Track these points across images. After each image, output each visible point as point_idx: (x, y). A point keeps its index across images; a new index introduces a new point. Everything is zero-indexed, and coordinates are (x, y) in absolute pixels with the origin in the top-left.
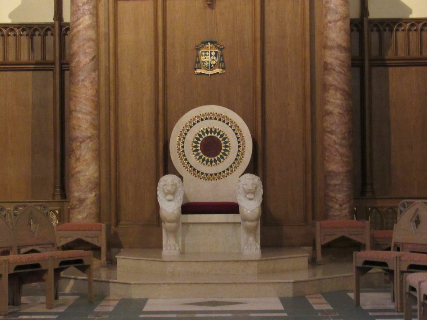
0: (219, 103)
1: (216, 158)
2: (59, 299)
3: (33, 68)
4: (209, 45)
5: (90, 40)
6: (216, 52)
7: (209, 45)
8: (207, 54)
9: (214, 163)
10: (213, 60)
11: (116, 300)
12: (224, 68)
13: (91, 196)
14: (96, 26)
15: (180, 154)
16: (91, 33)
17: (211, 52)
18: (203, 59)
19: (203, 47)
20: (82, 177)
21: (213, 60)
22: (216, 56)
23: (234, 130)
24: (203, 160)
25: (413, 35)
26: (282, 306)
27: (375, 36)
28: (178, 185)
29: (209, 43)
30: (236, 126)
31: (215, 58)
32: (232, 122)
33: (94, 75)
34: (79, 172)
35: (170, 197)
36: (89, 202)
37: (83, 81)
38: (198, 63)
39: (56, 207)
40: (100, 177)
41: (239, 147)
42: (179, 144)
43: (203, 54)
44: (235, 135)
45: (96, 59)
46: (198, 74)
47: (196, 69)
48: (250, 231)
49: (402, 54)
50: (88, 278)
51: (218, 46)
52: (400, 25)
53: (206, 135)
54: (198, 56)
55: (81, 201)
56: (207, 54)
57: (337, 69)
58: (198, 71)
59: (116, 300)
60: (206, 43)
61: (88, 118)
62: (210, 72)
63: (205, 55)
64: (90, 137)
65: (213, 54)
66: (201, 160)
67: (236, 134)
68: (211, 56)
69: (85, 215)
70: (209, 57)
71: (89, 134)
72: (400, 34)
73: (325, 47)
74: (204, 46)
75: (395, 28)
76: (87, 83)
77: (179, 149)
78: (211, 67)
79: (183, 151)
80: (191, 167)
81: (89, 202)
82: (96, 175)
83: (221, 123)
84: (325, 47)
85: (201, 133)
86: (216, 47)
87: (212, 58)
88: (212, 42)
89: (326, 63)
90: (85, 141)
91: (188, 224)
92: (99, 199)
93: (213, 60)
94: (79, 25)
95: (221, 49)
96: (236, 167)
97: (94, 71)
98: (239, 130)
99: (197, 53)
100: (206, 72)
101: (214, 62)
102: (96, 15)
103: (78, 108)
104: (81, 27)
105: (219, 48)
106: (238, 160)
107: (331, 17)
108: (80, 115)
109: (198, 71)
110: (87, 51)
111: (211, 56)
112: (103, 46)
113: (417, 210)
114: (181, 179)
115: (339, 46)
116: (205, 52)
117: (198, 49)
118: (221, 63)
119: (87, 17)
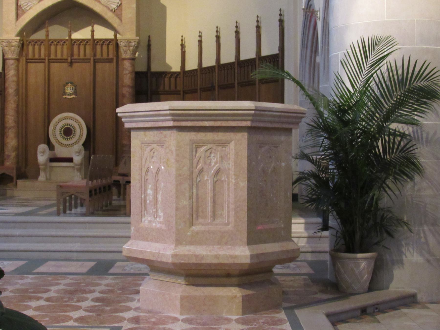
1: (70, 137)
2: (390, 289)
4: (69, 84)
5: (13, 81)
6: (73, 88)
7: (69, 84)
8: (68, 88)
9: (69, 140)
11: (301, 261)
12: (76, 95)
13: (14, 154)
14: (18, 75)
15: (53, 135)
16: (15, 79)
17: (70, 88)
18: (67, 91)
19: (67, 85)
20: (360, 165)
21: (71, 91)
22: (73, 89)
23: (78, 124)
24: (64, 138)
25: (173, 80)
27: (154, 79)
28: (46, 149)
29: (70, 84)
30: (79, 122)
31: (72, 90)
32: (77, 121)
33: (16, 98)
34: (8, 143)
35: (42, 154)
36: (12, 157)
37: (10, 101)
38: (64, 93)
40: (18, 145)
41: (81, 132)
42: (53, 131)
43: (67, 88)
44: (78, 127)
45: (17, 90)
46: (64, 98)
48: (79, 170)
49: (167, 88)
51: (74, 85)
52: (166, 75)
53: (65, 126)
54: (64, 89)
55: (9, 156)
56: (68, 88)
57: (127, 96)
58: (64, 97)
59: (301, 261)
60: (67, 83)
61: (13, 118)
62: (70, 97)
63: (68, 89)
64: (13, 127)
65: (71, 88)
66: (63, 138)
67: (79, 126)
68: (70, 89)
69: (10, 163)
70: (69, 90)
71: (13, 126)
72: (167, 80)
73: (123, 86)
75: (163, 76)
76: (12, 102)
77: (53, 133)
78: (70, 95)
79: (55, 134)
80: (58, 141)
81: (12, 157)
82: (16, 144)
83: (72, 121)
84: (123, 86)
85: (63, 126)
86: (73, 85)
87: (71, 90)
88: (71, 83)
89: (123, 94)
90: (10, 129)
91: (53, 167)
92: (17, 156)
93: (71, 91)
94: (9, 75)
95: (75, 86)
96: (79, 142)
97: (16, 96)
98: (80, 124)
99: (64, 88)
101: (71, 93)
102: (18, 70)
103: (8, 113)
104: (10, 75)
105: (74, 86)
106: (79, 139)
107: (125, 72)
108: (8, 117)
109: (64, 97)
110: (12, 87)
111: (70, 89)
112: (21, 84)
113: (126, 160)
115: (129, 86)
116: (68, 88)
117: (64, 86)
118: (75, 93)
119: (12, 71)
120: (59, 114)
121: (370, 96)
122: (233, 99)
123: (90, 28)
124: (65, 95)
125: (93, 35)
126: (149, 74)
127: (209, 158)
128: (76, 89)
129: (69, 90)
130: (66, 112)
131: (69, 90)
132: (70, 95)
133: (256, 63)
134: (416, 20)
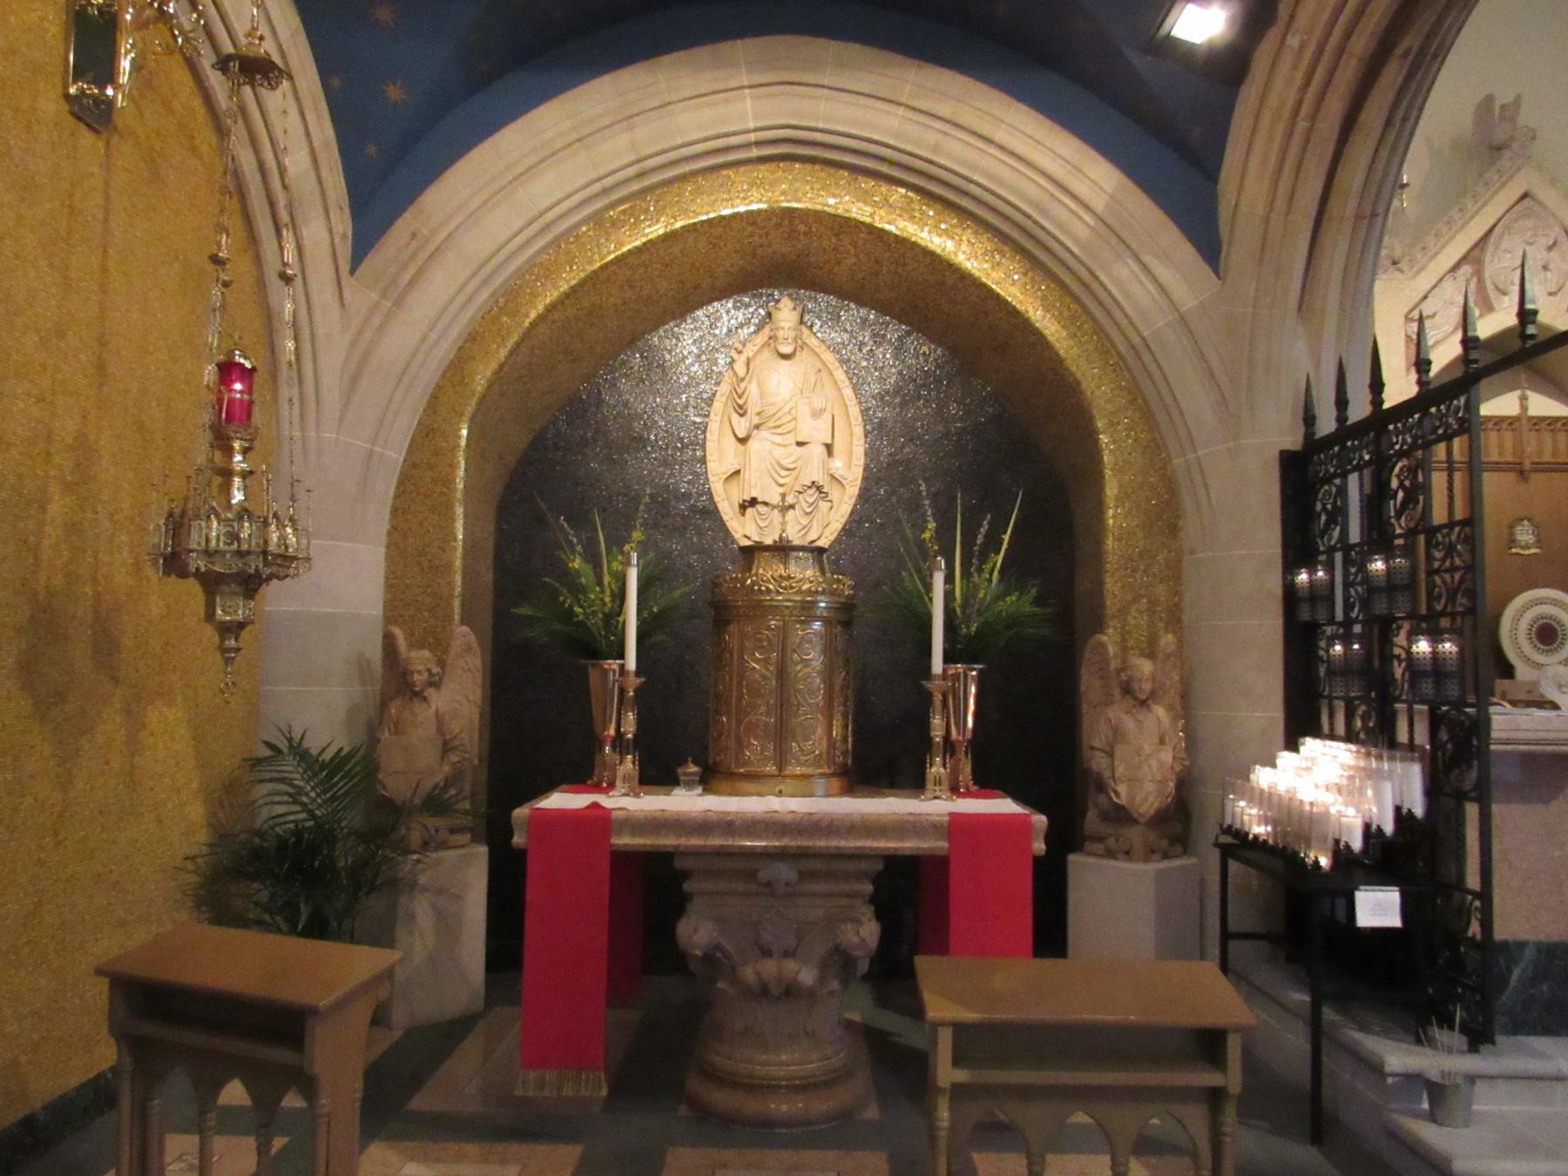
0: (1536, 586)
3: (1069, 321)
4: (1526, 522)
7: (1526, 522)
10: (1530, 538)
26: (1359, 419)
38: (1512, 542)
39: (453, 520)
46: (1512, 554)
47: (1510, 548)
49: (1495, 457)
50: (949, 842)
54: (1512, 534)
58: (1514, 550)
60: (1523, 520)
65: (1530, 532)
74: (1524, 342)
78: (1527, 547)
88: (1529, 520)
100: (1522, 552)
109: (1514, 550)
114: (565, 783)
117: (1511, 527)
118: (1539, 543)
120: (1545, 586)
121: (609, 740)
122: (638, 650)
123: (1518, 393)
124: (1515, 547)
125: (1524, 408)
126: (1524, 422)
127: (1551, 243)
128: (1538, 535)
129: (1525, 534)
130: (1518, 594)
131: (1525, 534)
132: (1527, 547)
133: (1550, 709)
134: (957, 1061)
